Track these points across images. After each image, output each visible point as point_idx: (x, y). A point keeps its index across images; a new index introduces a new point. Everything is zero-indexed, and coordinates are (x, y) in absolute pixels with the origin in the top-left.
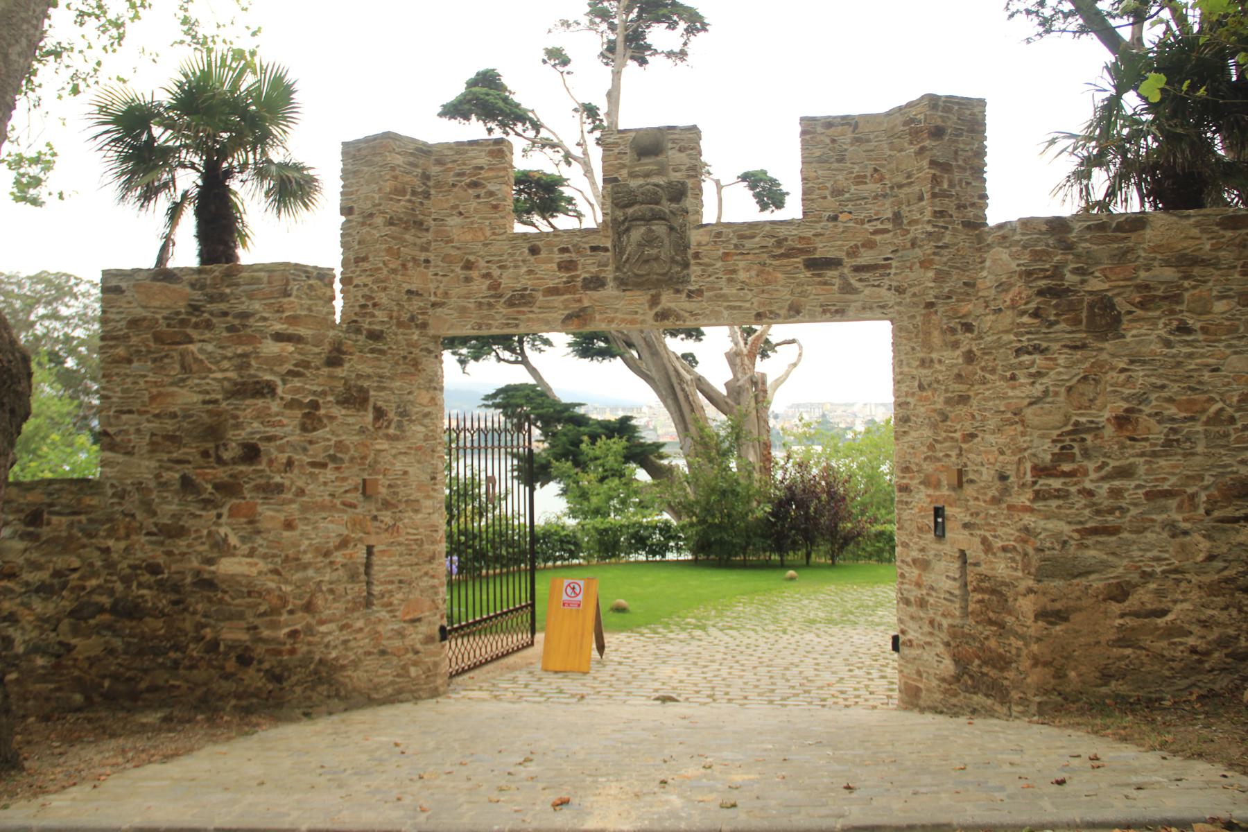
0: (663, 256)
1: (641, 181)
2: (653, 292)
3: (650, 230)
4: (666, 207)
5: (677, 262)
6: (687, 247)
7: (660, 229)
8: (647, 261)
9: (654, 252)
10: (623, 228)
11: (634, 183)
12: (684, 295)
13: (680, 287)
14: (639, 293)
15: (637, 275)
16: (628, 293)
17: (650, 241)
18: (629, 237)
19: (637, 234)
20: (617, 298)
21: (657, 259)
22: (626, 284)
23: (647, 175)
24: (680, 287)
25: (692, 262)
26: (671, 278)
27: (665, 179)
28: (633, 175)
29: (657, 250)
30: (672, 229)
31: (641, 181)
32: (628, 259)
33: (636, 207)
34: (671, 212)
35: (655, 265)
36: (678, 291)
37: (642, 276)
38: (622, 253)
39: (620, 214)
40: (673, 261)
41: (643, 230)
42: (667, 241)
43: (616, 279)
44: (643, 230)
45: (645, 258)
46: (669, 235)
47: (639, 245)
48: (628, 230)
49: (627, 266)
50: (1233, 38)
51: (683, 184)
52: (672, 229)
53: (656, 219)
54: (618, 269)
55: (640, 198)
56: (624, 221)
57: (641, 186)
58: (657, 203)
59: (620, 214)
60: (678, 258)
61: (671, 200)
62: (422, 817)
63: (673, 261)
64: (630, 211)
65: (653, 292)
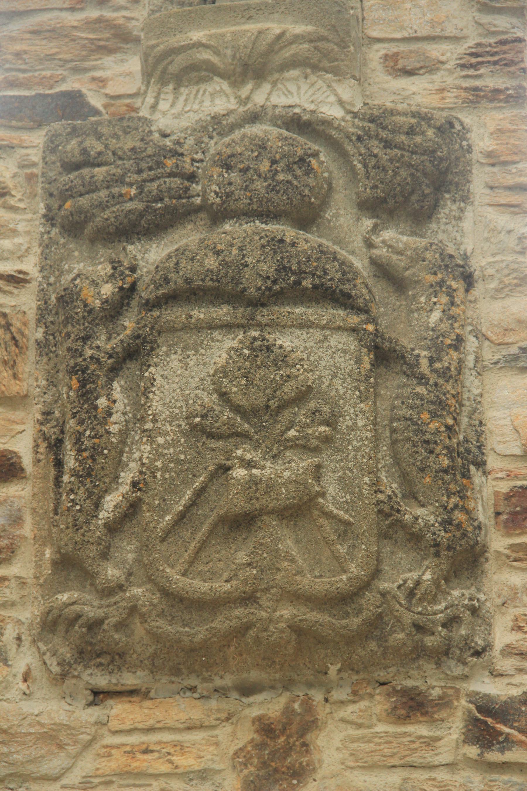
0: (333, 493)
1: (216, 100)
2: (270, 706)
3: (263, 352)
4: (350, 237)
5: (415, 538)
6: (469, 458)
7: (319, 349)
8: (240, 523)
9: (285, 470)
10: (105, 343)
11: (177, 114)
12: (451, 732)
13: (430, 681)
14: (183, 709)
15: (177, 602)
16: (119, 711)
17: (262, 408)
18: (141, 393)
19: (187, 375)
20: (52, 737)
21: (300, 510)
22: (116, 658)
23: (254, 67)
24: (430, 681)
25: (498, 542)
26: (376, 627)
27: (346, 91)
28: (173, 71)
29: (298, 464)
30: (384, 355)
31: (216, 100)
32: (131, 510)
33: (188, 236)
34: (383, 271)
35: (288, 541)
36: (414, 706)
37: (211, 605)
38: (94, 477)
39: (93, 274)
40: (391, 526)
41: (222, 349)
42: (356, 417)
43: (52, 624)
44: (222, 349)
45: (231, 500)
46: (369, 391)
47: (201, 430)
48: (136, 352)
49: (127, 550)
50: (326, 175)
51: (447, 128)
52: (384, 355)
53: (297, 294)
54: (68, 566)
55: (207, 189)
56: (114, 310)
57: (218, 125)
58: (307, 217)
59: (93, 274)
60: (423, 515)
61: (379, 206)
62: (343, 124)
63: (391, 526)
64: (151, 255)
65: (270, 706)
